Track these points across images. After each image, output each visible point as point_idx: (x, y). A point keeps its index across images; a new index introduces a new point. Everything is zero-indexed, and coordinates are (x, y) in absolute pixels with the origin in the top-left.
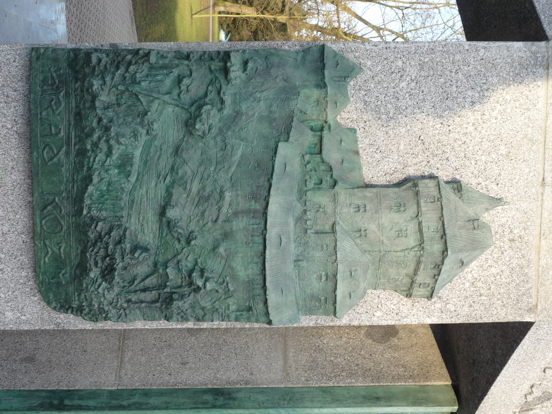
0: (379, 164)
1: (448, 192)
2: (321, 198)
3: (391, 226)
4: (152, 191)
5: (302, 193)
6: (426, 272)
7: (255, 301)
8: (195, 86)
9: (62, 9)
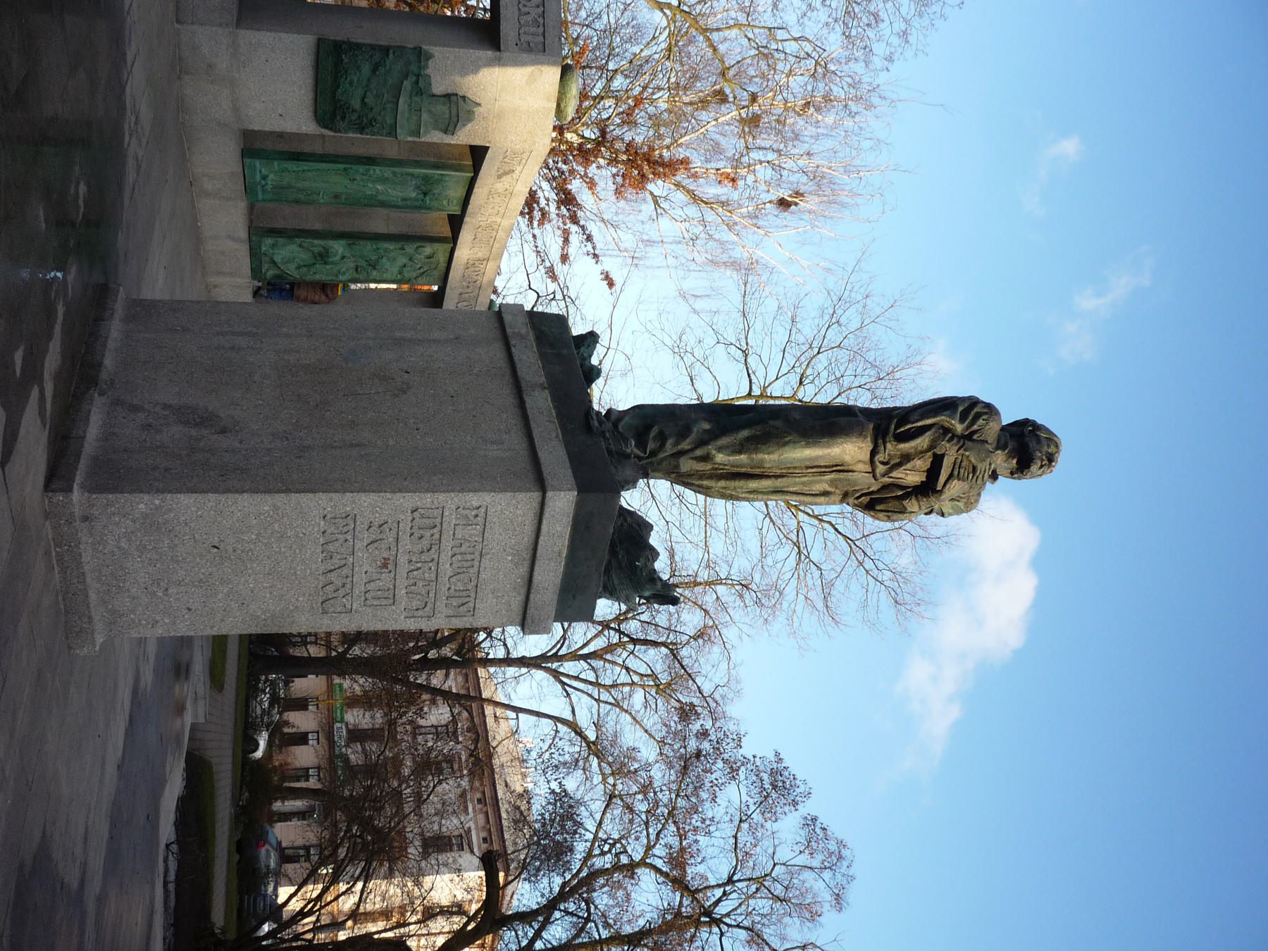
0: (438, 88)
1: (460, 100)
2: (417, 99)
3: (441, 109)
4: (360, 92)
5: (411, 97)
6: (450, 127)
7: (392, 132)
8: (377, 57)
9: (560, 554)
